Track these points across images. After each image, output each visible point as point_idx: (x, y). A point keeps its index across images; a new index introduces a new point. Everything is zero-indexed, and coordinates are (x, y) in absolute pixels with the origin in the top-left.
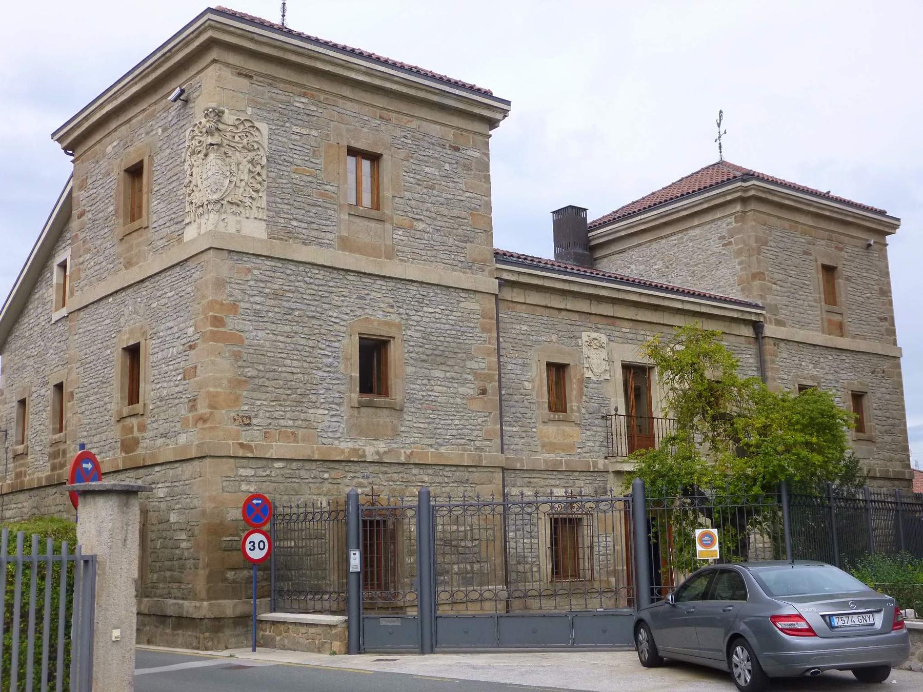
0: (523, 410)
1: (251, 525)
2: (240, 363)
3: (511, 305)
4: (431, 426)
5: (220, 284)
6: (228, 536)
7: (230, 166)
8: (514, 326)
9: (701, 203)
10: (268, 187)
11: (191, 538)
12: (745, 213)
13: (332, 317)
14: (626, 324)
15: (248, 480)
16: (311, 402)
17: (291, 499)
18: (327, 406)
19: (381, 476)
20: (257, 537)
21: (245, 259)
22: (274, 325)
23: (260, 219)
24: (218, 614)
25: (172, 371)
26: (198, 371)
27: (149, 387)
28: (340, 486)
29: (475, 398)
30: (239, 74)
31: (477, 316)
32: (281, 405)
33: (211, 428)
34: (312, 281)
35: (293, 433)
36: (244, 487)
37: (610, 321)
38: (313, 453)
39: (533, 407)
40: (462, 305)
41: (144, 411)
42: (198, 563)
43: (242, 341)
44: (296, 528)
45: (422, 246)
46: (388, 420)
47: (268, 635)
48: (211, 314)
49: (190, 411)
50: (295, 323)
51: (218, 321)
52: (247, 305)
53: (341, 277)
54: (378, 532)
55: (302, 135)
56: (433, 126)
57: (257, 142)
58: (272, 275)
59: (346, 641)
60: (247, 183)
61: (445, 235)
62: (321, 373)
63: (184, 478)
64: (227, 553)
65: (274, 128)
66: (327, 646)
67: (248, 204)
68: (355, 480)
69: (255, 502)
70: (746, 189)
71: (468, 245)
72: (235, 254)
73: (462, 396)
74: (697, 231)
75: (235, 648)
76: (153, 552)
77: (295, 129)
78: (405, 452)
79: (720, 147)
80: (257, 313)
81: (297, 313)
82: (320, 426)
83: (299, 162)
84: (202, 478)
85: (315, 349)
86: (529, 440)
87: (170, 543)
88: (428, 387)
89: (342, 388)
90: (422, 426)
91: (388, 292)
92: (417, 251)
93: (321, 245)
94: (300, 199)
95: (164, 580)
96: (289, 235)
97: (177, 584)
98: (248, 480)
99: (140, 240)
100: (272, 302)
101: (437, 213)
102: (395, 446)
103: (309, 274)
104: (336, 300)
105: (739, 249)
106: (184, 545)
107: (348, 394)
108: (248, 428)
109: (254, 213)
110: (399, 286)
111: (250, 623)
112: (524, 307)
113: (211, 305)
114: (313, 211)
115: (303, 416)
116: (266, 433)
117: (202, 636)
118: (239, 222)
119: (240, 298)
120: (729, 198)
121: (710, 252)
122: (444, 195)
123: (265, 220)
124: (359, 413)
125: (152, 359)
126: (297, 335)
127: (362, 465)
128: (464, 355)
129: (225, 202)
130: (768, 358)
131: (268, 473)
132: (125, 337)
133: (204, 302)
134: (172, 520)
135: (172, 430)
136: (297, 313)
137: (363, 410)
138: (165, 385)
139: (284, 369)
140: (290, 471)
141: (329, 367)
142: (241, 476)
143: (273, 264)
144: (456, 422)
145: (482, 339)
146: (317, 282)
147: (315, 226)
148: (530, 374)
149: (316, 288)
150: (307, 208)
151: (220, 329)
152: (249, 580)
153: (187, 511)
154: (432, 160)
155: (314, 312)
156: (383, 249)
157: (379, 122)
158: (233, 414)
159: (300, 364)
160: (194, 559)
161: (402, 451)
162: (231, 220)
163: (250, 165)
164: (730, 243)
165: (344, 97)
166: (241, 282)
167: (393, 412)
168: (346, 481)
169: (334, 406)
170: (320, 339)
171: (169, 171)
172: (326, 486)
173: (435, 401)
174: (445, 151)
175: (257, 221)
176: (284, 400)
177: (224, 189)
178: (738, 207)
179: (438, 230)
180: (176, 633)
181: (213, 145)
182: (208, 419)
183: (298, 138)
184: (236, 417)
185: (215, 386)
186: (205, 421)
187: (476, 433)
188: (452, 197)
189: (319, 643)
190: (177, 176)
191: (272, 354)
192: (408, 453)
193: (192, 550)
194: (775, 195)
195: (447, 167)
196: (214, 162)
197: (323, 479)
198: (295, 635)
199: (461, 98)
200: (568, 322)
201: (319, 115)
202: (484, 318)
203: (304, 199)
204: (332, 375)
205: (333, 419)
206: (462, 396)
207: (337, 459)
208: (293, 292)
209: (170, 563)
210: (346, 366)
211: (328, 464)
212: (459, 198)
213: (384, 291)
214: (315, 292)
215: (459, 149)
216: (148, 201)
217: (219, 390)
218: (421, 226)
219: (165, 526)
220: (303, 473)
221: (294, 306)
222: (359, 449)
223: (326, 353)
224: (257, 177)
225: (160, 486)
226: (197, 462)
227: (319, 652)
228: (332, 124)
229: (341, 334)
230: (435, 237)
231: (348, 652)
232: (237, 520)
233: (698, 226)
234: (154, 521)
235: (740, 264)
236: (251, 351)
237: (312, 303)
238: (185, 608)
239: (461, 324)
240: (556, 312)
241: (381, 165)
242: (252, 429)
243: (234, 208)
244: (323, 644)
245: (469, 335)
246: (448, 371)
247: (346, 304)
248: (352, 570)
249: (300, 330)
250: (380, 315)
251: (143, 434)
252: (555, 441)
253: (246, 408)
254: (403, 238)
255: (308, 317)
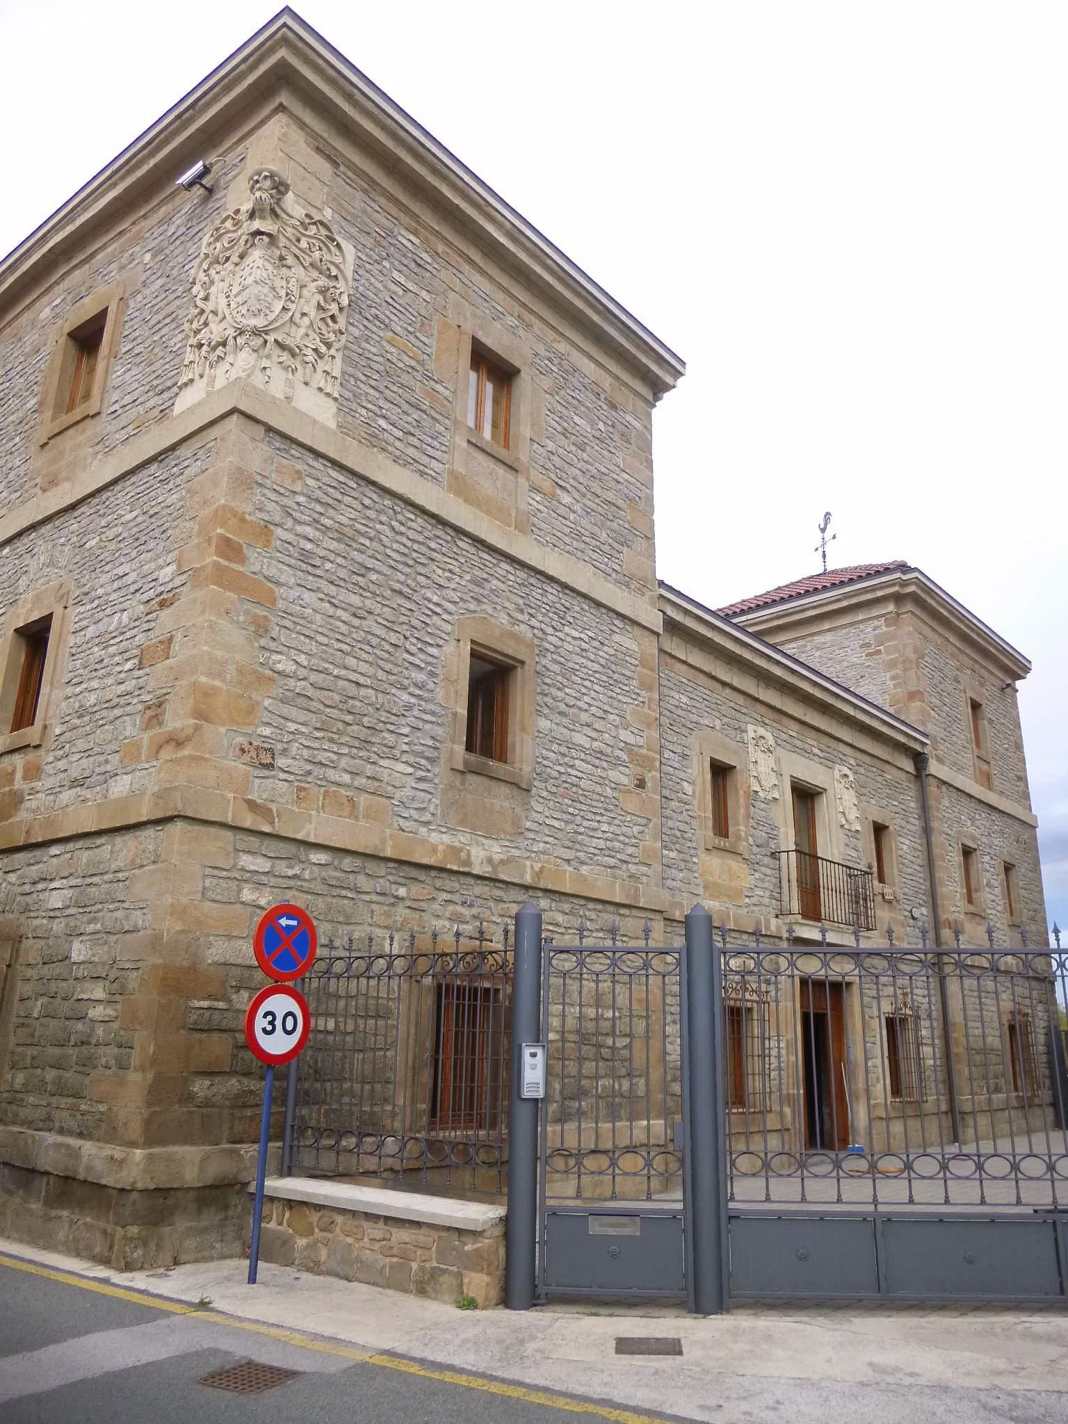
0: (683, 826)
1: (268, 972)
2: (263, 642)
3: (669, 660)
4: (569, 828)
5: (244, 481)
6: (203, 999)
7: (288, 282)
8: (673, 693)
9: (839, 600)
10: (346, 348)
11: (117, 998)
12: (898, 615)
13: (430, 601)
14: (792, 724)
15: (255, 879)
16: (385, 745)
17: (337, 930)
18: (412, 759)
19: (491, 904)
20: (281, 1004)
21: (293, 452)
22: (333, 588)
23: (328, 395)
24: (163, 1181)
25: (114, 655)
26: (176, 646)
27: (59, 694)
28: (426, 916)
29: (631, 792)
30: (318, 150)
31: (634, 661)
32: (332, 741)
33: (192, 758)
34: (403, 529)
35: (350, 800)
36: (247, 895)
37: (777, 716)
38: (383, 841)
39: (695, 823)
40: (617, 638)
41: (42, 739)
42: (130, 1055)
43: (274, 601)
44: (342, 992)
45: (567, 530)
46: (506, 804)
47: (274, 1231)
48: (219, 531)
49: (148, 726)
50: (368, 594)
51: (230, 549)
52: (289, 537)
53: (449, 538)
54: (486, 1009)
55: (406, 290)
56: (586, 361)
57: (337, 266)
58: (339, 497)
59: (500, 1273)
60: (312, 323)
61: (595, 524)
62: (406, 697)
63: (114, 866)
64: (198, 1035)
65: (364, 258)
66: (446, 1280)
67: (309, 359)
68: (451, 908)
69: (284, 922)
70: (904, 584)
71: (625, 549)
72: (277, 438)
73: (613, 785)
74: (828, 637)
75: (196, 1261)
76: (23, 1025)
77: (396, 275)
78: (532, 867)
79: (824, 556)
80: (305, 556)
81: (374, 577)
82: (398, 794)
83: (398, 329)
84: (159, 865)
85: (400, 650)
86: (690, 875)
87: (65, 1008)
88: (566, 760)
89: (439, 731)
90: (556, 823)
91: (516, 585)
92: (559, 534)
93: (422, 473)
94: (395, 389)
95: (40, 1088)
96: (373, 440)
97: (70, 1100)
98: (255, 879)
99: (80, 438)
100: (334, 545)
101: (588, 488)
102: (516, 853)
103: (400, 517)
104: (439, 575)
105: (891, 659)
106: (96, 1012)
107: (448, 744)
108: (267, 773)
109: (319, 380)
110: (532, 580)
111: (234, 1200)
112: (684, 667)
113: (223, 515)
114: (414, 416)
115: (369, 770)
116: (300, 789)
117: (120, 1231)
118: (289, 383)
119: (277, 519)
120: (880, 594)
121: (846, 664)
122: (597, 465)
123: (335, 399)
124: (463, 783)
125: (72, 640)
126: (370, 617)
127: (463, 879)
128: (618, 719)
129: (271, 338)
130: (932, 803)
131: (297, 871)
132: (22, 611)
133: (207, 512)
134: (75, 957)
135: (98, 770)
136: (374, 577)
137: (471, 778)
138: (95, 684)
139: (343, 672)
140: (337, 874)
141: (420, 688)
142: (243, 869)
143: (342, 479)
144: (605, 827)
145: (641, 699)
146: (411, 534)
147: (415, 441)
148: (690, 771)
149: (409, 544)
150: (406, 407)
151: (234, 566)
152: (240, 1102)
153: (113, 938)
154: (583, 409)
155: (402, 583)
156: (514, 515)
157: (518, 324)
158: (240, 739)
159: (371, 671)
160: (120, 1046)
161: (528, 863)
162: (278, 375)
163: (321, 298)
164: (878, 652)
165: (471, 262)
166: (282, 491)
167: (516, 791)
168: (436, 906)
169: (423, 762)
170: (408, 634)
171: (157, 312)
172: (401, 913)
173: (576, 786)
174: (600, 403)
175: (322, 395)
176: (339, 732)
177: (271, 317)
178: (891, 607)
179: (588, 513)
180: (53, 1213)
181: (262, 233)
182: (188, 739)
183: (401, 292)
184: (246, 746)
185: (210, 674)
186: (179, 744)
187: (630, 850)
188: (607, 471)
189: (422, 1269)
190: (174, 315)
191: (325, 640)
192: (537, 869)
193: (115, 1025)
194: (932, 598)
195: (601, 425)
196: (260, 263)
197: (396, 897)
198: (349, 1240)
199: (627, 332)
200: (732, 705)
201: (434, 272)
202: (643, 667)
203: (401, 391)
204: (423, 703)
205: (422, 786)
206: (613, 785)
207: (425, 861)
208: (371, 539)
209: (58, 1051)
210: (447, 693)
211: (406, 868)
212: (616, 477)
213: (511, 583)
214: (406, 551)
215: (616, 408)
216: (107, 371)
217: (218, 683)
218: (566, 499)
219: (57, 969)
220: (362, 881)
221: (370, 563)
222: (461, 850)
223: (418, 662)
224: (329, 321)
225: (53, 885)
226: (150, 832)
227: (422, 1292)
228: (452, 295)
229: (443, 635)
230: (583, 522)
231: (506, 1300)
232: (225, 964)
233: (829, 630)
234: (33, 957)
235: (893, 678)
236: (288, 624)
237: (400, 567)
238: (85, 1160)
239: (614, 667)
240: (718, 687)
241: (513, 388)
242: (273, 777)
243: (285, 357)
244: (435, 1274)
245: (624, 688)
246: (596, 740)
247: (453, 586)
248: (527, 1093)
249: (377, 609)
250: (504, 619)
251: (33, 785)
252: (720, 881)
253: (267, 731)
254: (541, 507)
255: (394, 591)
